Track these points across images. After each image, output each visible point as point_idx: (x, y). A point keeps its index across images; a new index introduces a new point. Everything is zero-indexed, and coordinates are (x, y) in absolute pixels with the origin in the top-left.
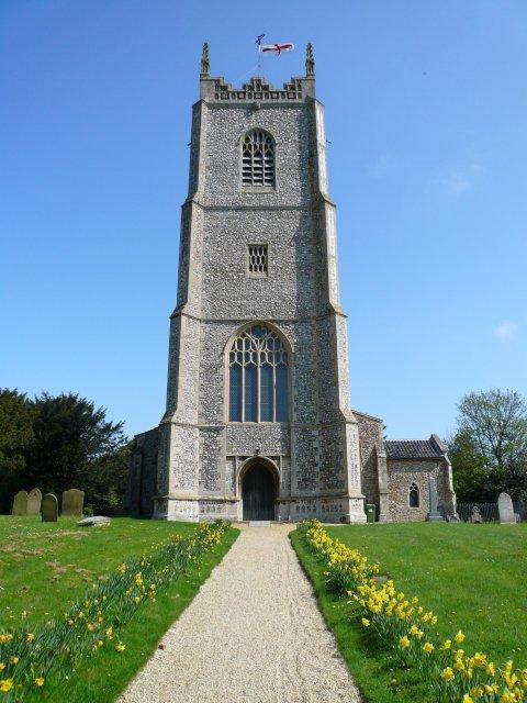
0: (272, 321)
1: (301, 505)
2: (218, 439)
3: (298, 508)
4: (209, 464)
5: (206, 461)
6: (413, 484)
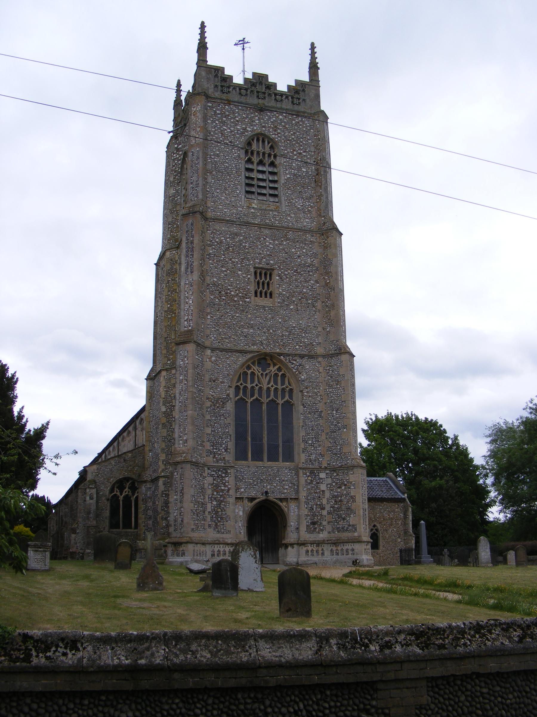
0: (280, 354)
1: (310, 548)
2: (227, 479)
3: (307, 551)
4: (219, 506)
5: (215, 503)
6: (374, 526)
